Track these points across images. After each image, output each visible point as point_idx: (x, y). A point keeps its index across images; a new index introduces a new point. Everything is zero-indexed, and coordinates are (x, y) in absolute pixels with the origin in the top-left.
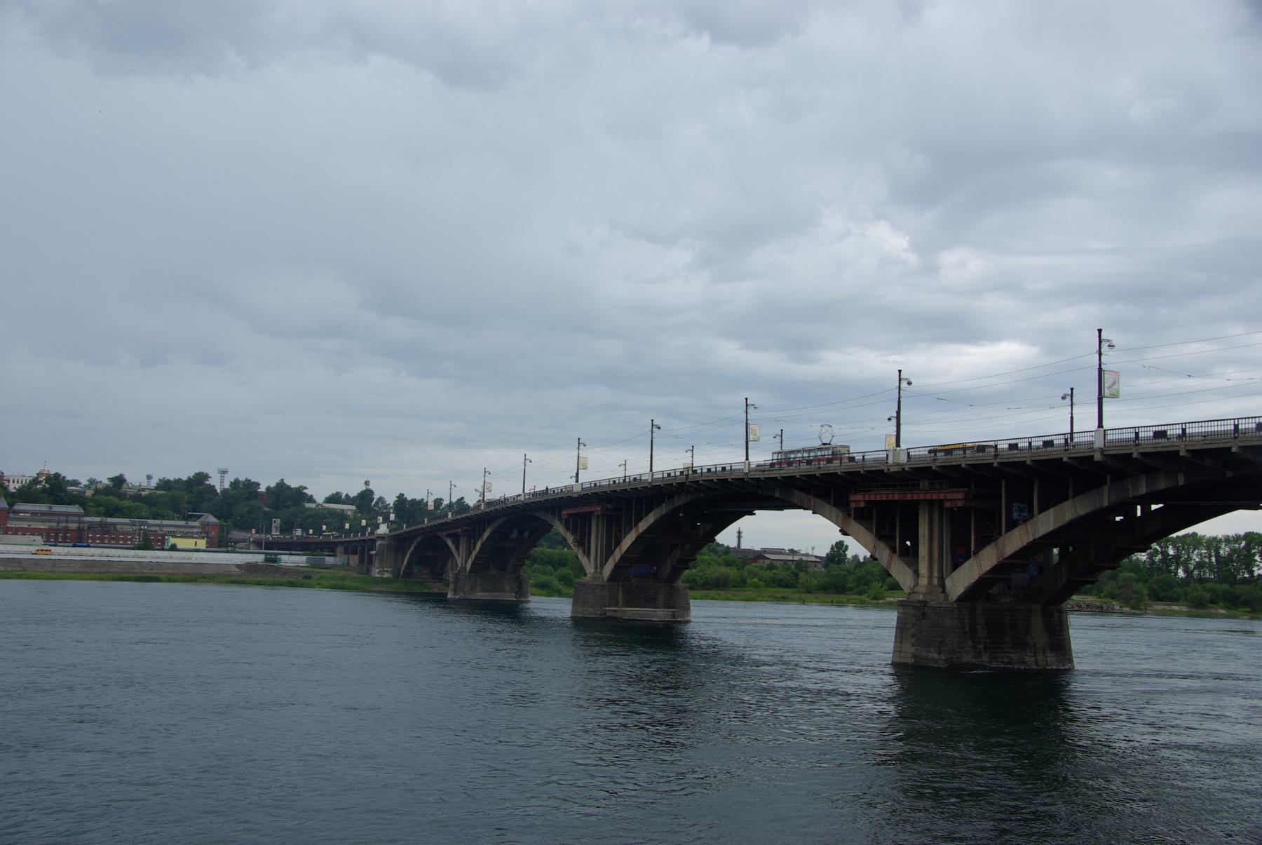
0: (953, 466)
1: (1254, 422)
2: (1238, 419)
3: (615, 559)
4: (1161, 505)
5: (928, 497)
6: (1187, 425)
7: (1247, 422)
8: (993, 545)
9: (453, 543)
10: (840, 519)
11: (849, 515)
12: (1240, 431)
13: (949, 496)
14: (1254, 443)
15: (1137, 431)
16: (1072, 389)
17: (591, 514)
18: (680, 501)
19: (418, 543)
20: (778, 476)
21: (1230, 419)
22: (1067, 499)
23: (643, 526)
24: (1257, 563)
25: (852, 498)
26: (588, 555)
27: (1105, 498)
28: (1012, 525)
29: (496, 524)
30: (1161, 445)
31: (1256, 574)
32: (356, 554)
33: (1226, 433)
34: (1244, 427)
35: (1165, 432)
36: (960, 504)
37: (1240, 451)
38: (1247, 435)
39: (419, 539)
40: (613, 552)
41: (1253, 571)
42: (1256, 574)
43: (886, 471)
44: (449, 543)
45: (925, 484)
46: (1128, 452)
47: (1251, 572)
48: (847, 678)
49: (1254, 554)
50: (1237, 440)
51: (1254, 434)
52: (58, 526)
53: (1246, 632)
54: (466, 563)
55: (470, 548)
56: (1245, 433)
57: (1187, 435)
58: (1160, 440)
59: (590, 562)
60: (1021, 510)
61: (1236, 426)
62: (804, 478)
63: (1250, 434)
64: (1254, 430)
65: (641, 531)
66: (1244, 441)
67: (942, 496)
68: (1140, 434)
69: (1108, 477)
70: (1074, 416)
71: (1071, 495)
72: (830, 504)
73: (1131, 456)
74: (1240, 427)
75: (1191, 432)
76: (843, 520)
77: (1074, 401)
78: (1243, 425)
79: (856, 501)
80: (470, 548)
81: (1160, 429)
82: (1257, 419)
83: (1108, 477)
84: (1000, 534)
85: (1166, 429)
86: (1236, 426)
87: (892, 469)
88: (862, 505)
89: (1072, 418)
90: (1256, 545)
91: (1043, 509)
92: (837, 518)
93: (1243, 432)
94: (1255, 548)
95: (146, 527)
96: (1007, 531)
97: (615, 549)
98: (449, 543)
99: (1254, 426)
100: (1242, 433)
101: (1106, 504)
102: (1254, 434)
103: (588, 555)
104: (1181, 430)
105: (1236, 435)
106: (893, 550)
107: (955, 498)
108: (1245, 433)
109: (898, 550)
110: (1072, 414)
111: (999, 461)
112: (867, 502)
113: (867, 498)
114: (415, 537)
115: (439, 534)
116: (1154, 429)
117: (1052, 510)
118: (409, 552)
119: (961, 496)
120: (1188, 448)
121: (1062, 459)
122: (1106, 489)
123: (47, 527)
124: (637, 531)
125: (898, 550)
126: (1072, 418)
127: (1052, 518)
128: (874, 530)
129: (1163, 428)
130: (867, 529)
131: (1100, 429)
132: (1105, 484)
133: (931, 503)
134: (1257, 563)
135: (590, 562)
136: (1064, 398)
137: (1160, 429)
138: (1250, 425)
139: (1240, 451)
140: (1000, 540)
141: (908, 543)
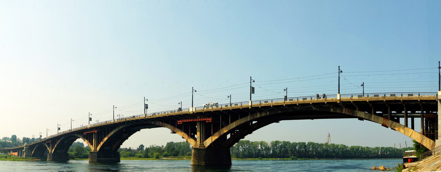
3: (101, 145)
4: (256, 122)
5: (199, 120)
8: (218, 132)
9: (48, 145)
10: (172, 128)
11: (175, 127)
13: (207, 119)
15: (368, 94)
16: (363, 83)
17: (92, 133)
18: (121, 127)
19: (35, 150)
20: (155, 117)
22: (238, 119)
23: (110, 135)
25: (178, 121)
26: (92, 145)
27: (249, 118)
28: (223, 127)
29: (61, 139)
30: (267, 104)
32: (17, 152)
36: (211, 121)
39: (37, 146)
40: (100, 143)
43: (189, 114)
44: (46, 146)
45: (198, 117)
46: (258, 106)
54: (52, 151)
55: (53, 146)
59: (93, 147)
60: (225, 123)
61: (385, 95)
62: (163, 118)
65: (109, 137)
67: (205, 120)
69: (250, 114)
71: (239, 118)
72: (169, 124)
76: (173, 128)
79: (179, 122)
80: (53, 146)
83: (250, 114)
84: (220, 129)
86: (385, 95)
87: (191, 113)
88: (181, 123)
91: (232, 122)
92: (171, 128)
96: (221, 129)
97: (101, 142)
98: (46, 146)
101: (249, 120)
103: (92, 145)
106: (188, 135)
107: (209, 120)
109: (190, 135)
110: (363, 90)
111: (222, 109)
112: (182, 122)
113: (183, 121)
114: (36, 146)
115: (44, 144)
117: (234, 122)
118: (34, 150)
119: (211, 119)
120: (273, 105)
122: (249, 116)
124: (103, 142)
125: (190, 135)
127: (249, 118)
128: (183, 130)
130: (181, 130)
132: (249, 115)
133: (200, 122)
135: (93, 147)
140: (220, 131)
141: (192, 134)
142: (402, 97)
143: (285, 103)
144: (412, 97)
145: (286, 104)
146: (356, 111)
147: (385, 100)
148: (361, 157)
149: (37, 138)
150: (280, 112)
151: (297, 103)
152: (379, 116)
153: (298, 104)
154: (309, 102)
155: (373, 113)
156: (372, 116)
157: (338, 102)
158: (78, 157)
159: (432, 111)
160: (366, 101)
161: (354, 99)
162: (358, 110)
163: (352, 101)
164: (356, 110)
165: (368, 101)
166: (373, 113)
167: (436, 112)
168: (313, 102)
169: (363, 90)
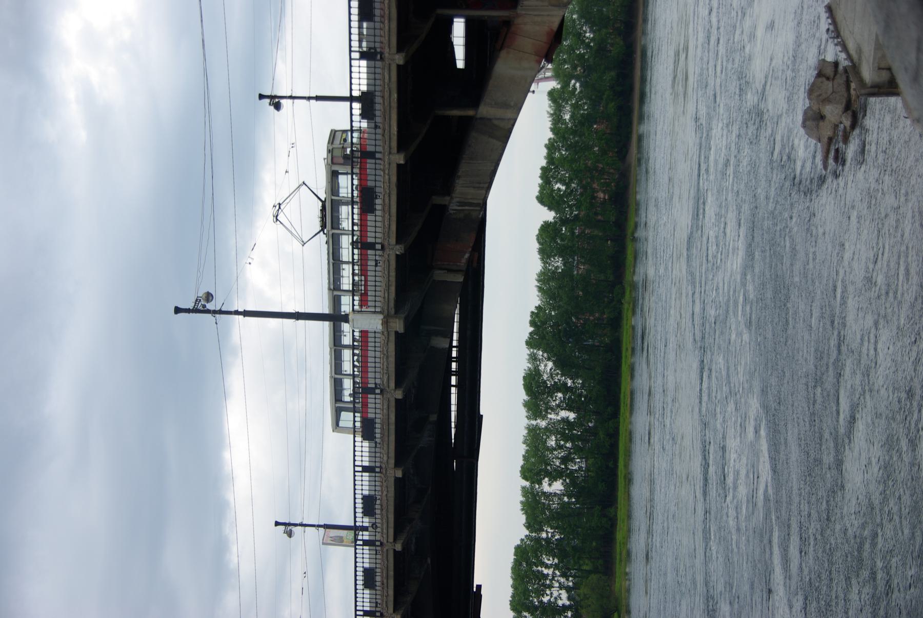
0: (399, 132)
1: (362, 592)
2: (355, 466)
6: (357, 463)
7: (360, 483)
12: (373, 609)
14: (391, 592)
15: (360, 469)
16: (277, 524)
21: (351, 66)
24: (552, 600)
31: (568, 603)
33: (373, 455)
34: (368, 604)
35: (366, 571)
37: (401, 612)
38: (379, 601)
41: (563, 605)
42: (568, 603)
47: (565, 608)
48: (842, 416)
49: (541, 602)
50: (385, 614)
51: (378, 592)
52: (358, 225)
53: (722, 71)
56: (376, 603)
57: (373, 464)
58: (378, 431)
61: (365, 469)
63: (378, 597)
64: (374, 592)
66: (387, 606)
68: (366, 609)
70: (322, 523)
73: (398, 552)
74: (368, 609)
75: (367, 459)
77: (298, 522)
78: (364, 459)
81: (360, 578)
82: (354, 118)
85: (360, 496)
86: (365, 469)
89: (318, 98)
90: (528, 599)
93: (374, 605)
94: (532, 601)
95: (569, 383)
99: (367, 591)
100: (376, 607)
102: (378, 592)
104: (364, 474)
105: (378, 543)
108: (376, 603)
110: (309, 98)
116: (360, 587)
121: (397, 400)
123: (777, 528)
126: (318, 98)
129: (360, 574)
131: (350, 317)
134: (552, 600)
136: (290, 534)
137: (361, 578)
138: (364, 449)
139: (401, 612)
142: (381, 467)
143: (382, 544)
144: (378, 426)
145: (392, 385)
146: (453, 207)
147: (397, 57)
148: (573, 442)
149: (552, 130)
150: (429, 561)
151: (388, 546)
152: (492, 83)
153: (395, 540)
154: (392, 480)
155: (471, 113)
156: (490, 120)
157: (398, 325)
158: (563, 467)
159: (457, 373)
160: (399, 166)
161: (387, 234)
162: (448, 198)
163: (399, 250)
164: (444, 208)
165: (400, 159)
166: (471, 113)
167: (455, 384)
168: (392, 461)
169: (309, 98)
